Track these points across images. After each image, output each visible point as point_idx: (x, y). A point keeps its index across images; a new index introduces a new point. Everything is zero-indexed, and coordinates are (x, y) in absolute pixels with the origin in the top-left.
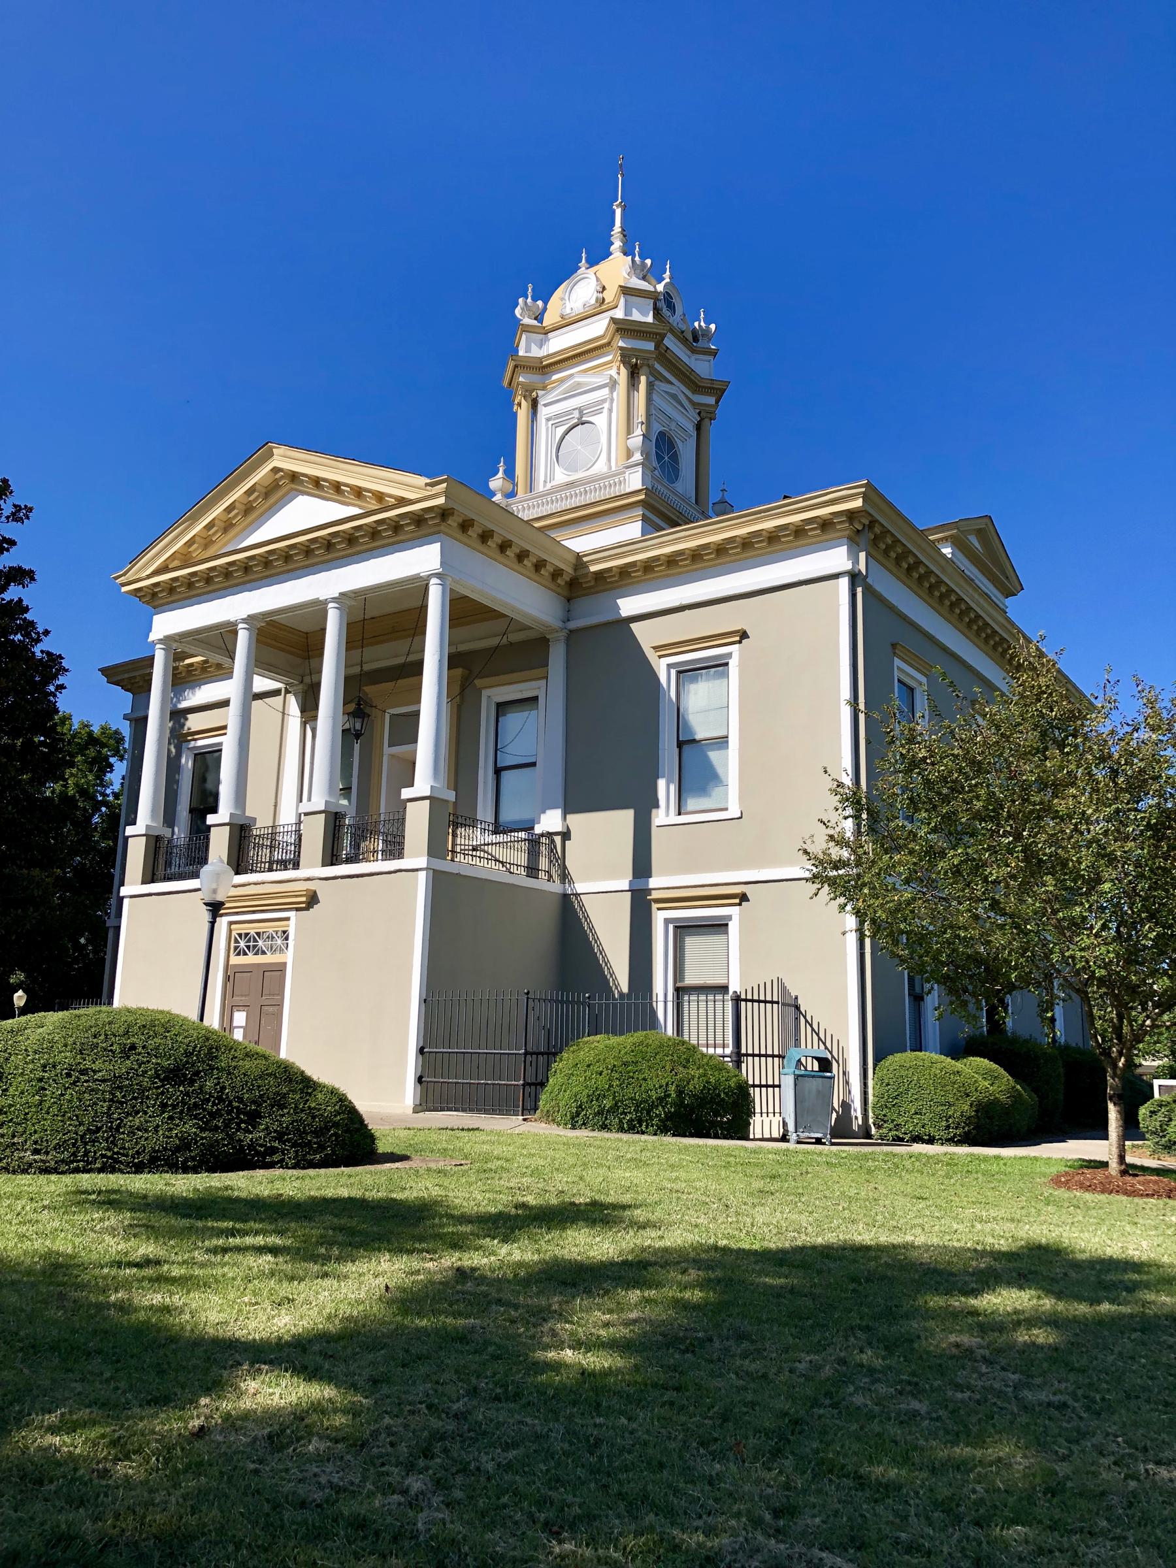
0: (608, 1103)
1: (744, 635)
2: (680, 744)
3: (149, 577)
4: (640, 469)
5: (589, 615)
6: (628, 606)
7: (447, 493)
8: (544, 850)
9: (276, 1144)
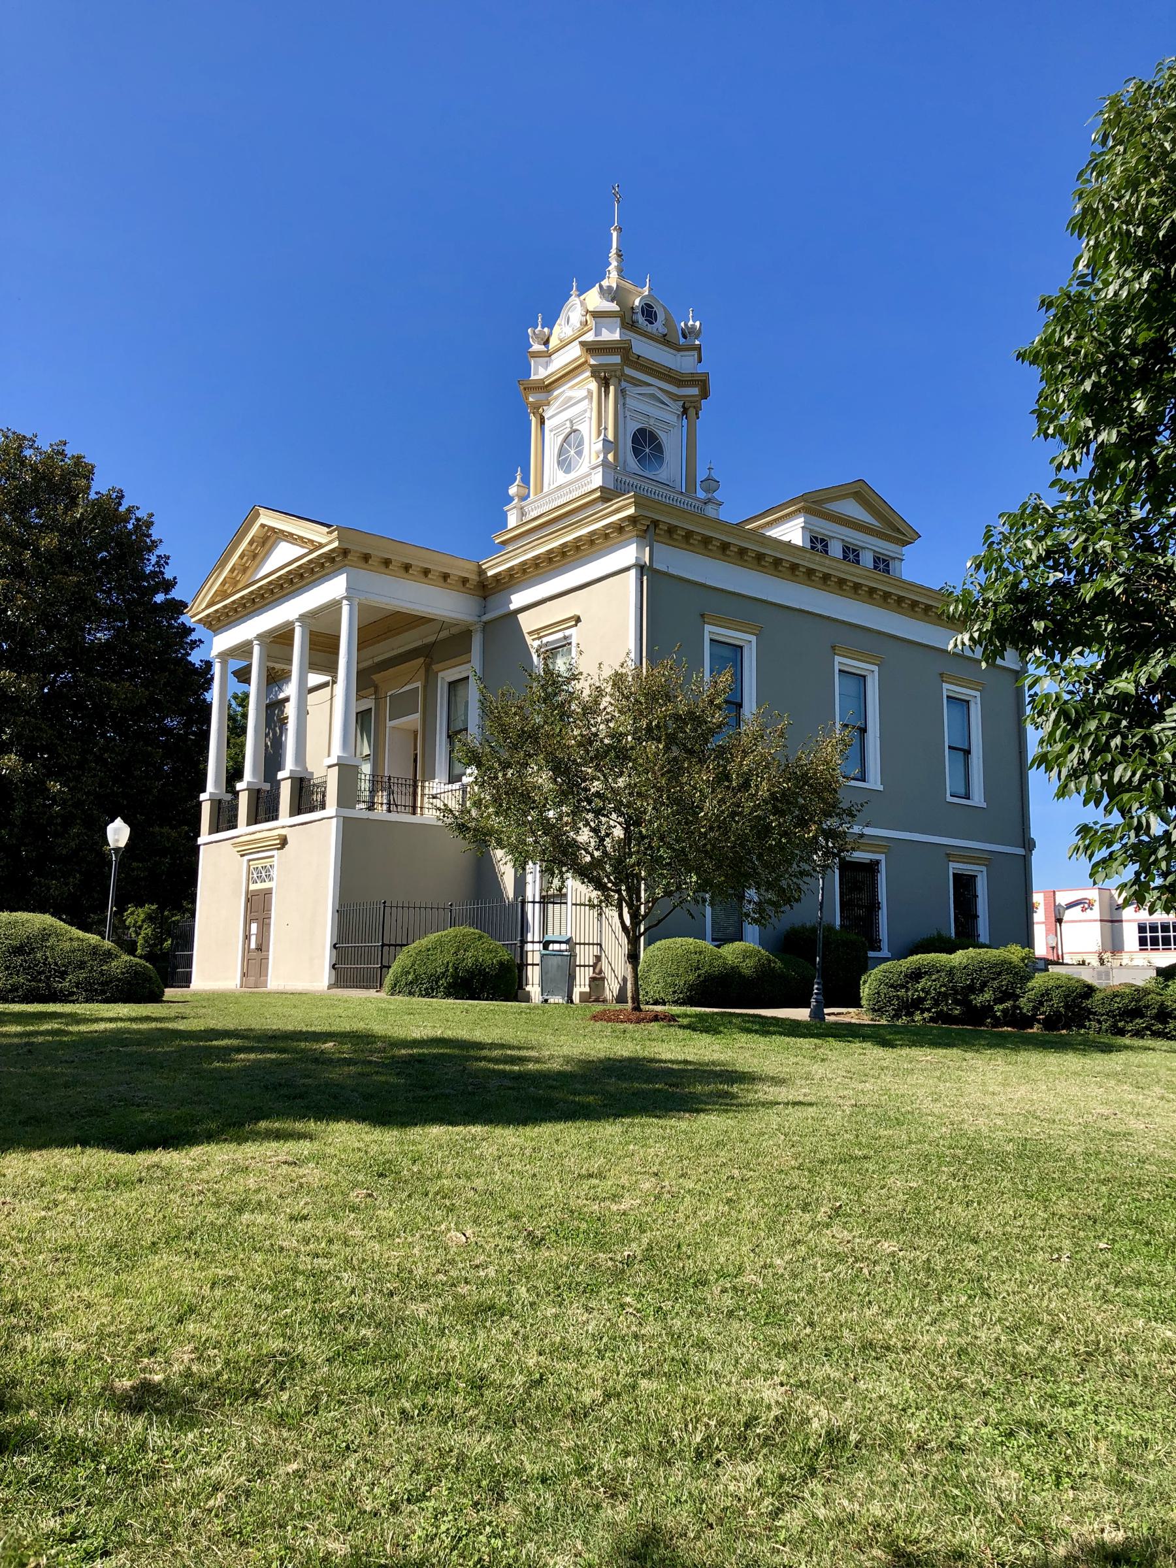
1: (578, 620)
6: (518, 600)
7: (339, 538)
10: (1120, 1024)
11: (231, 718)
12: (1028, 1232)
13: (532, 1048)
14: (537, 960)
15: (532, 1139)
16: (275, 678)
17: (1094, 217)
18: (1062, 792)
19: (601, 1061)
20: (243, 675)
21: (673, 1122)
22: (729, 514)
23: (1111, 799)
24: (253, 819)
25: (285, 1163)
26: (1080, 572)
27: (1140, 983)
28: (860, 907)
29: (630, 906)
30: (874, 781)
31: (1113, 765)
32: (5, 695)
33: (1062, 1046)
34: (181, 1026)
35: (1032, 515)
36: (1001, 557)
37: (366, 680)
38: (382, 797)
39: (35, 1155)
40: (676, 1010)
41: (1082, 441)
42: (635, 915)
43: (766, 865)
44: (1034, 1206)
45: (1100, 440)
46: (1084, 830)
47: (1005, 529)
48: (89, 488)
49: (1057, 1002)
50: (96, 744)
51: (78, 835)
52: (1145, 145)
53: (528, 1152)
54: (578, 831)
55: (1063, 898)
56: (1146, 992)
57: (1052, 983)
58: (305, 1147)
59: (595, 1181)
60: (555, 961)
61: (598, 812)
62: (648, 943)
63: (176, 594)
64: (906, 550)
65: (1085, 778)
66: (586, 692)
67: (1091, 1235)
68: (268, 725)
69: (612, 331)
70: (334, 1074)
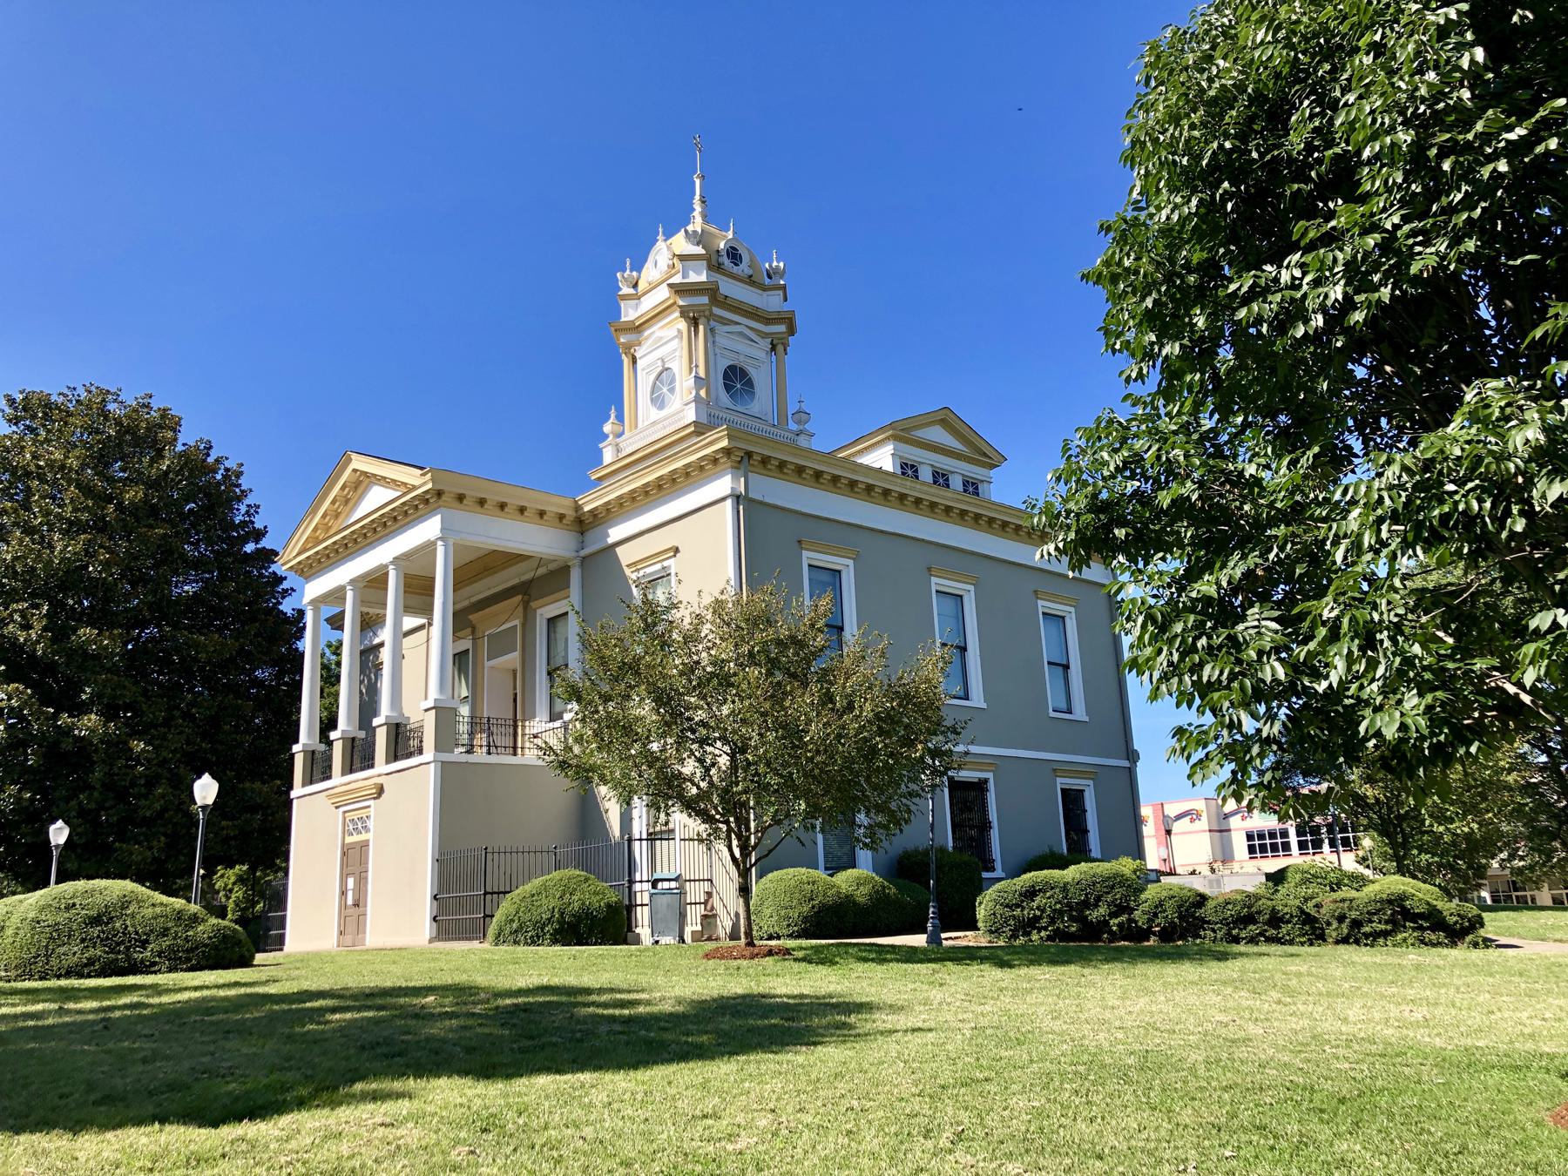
1: (677, 550)
3: (299, 554)
6: (615, 533)
7: (433, 480)
10: (1235, 932)
11: (325, 667)
12: (1153, 1145)
13: (643, 991)
14: (646, 901)
15: (643, 1083)
16: (369, 624)
17: (1142, 150)
18: (1155, 695)
19: (714, 1000)
20: (336, 622)
21: (790, 1056)
22: (820, 444)
23: (1202, 698)
24: (349, 768)
25: (382, 1125)
26: (1156, 480)
27: (1250, 889)
28: (972, 828)
29: (739, 837)
30: (977, 699)
31: (1201, 665)
32: (85, 652)
33: (1179, 956)
34: (272, 989)
35: (1106, 428)
36: (1080, 469)
37: (462, 620)
38: (481, 739)
39: (110, 1135)
40: (791, 943)
41: (1149, 355)
42: (744, 847)
43: (875, 788)
44: (1158, 1118)
45: (1164, 353)
46: (1179, 732)
47: (1082, 443)
48: (176, 440)
49: (1171, 913)
50: (183, 700)
51: (163, 796)
52: (1183, 84)
53: (639, 1097)
54: (682, 761)
55: (1172, 810)
56: (1257, 897)
57: (1164, 894)
58: (404, 1106)
59: (710, 1122)
60: (665, 899)
61: (703, 742)
62: (760, 876)
63: (266, 543)
64: (993, 472)
65: (1176, 680)
66: (687, 620)
67: (1216, 1143)
68: (362, 672)
69: (698, 273)
70: (435, 1029)
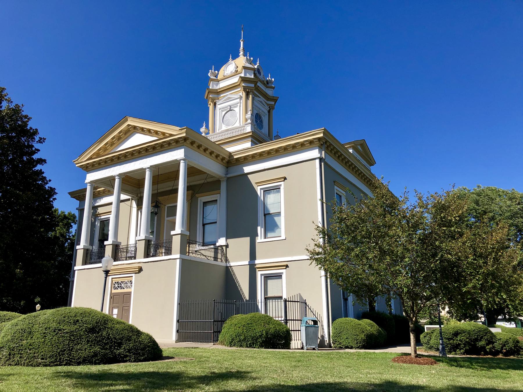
0: (242, 338)
1: (285, 179)
2: (265, 215)
3: (85, 161)
4: (250, 125)
5: (234, 172)
6: (247, 169)
7: (186, 132)
8: (219, 251)
9: (128, 354)
